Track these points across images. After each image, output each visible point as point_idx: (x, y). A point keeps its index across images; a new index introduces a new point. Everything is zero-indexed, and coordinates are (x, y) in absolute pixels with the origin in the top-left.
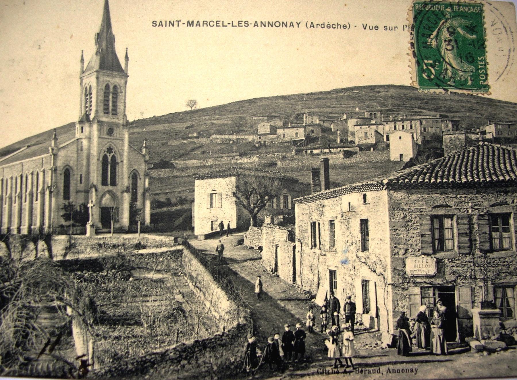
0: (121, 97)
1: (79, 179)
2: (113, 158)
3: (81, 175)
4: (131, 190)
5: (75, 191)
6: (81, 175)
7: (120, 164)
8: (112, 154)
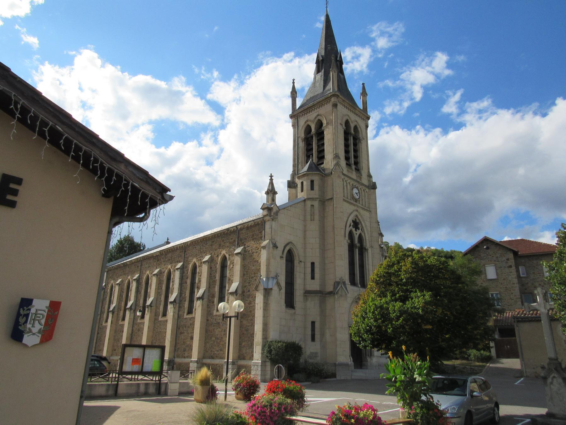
0: (362, 146)
1: (309, 270)
2: (360, 238)
3: (313, 264)
4: (484, 364)
5: (302, 292)
6: (313, 264)
7: (370, 251)
8: (359, 232)
